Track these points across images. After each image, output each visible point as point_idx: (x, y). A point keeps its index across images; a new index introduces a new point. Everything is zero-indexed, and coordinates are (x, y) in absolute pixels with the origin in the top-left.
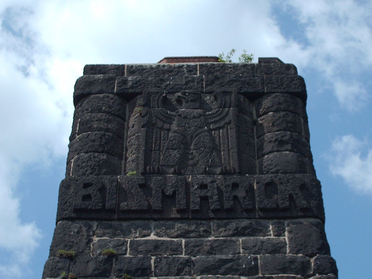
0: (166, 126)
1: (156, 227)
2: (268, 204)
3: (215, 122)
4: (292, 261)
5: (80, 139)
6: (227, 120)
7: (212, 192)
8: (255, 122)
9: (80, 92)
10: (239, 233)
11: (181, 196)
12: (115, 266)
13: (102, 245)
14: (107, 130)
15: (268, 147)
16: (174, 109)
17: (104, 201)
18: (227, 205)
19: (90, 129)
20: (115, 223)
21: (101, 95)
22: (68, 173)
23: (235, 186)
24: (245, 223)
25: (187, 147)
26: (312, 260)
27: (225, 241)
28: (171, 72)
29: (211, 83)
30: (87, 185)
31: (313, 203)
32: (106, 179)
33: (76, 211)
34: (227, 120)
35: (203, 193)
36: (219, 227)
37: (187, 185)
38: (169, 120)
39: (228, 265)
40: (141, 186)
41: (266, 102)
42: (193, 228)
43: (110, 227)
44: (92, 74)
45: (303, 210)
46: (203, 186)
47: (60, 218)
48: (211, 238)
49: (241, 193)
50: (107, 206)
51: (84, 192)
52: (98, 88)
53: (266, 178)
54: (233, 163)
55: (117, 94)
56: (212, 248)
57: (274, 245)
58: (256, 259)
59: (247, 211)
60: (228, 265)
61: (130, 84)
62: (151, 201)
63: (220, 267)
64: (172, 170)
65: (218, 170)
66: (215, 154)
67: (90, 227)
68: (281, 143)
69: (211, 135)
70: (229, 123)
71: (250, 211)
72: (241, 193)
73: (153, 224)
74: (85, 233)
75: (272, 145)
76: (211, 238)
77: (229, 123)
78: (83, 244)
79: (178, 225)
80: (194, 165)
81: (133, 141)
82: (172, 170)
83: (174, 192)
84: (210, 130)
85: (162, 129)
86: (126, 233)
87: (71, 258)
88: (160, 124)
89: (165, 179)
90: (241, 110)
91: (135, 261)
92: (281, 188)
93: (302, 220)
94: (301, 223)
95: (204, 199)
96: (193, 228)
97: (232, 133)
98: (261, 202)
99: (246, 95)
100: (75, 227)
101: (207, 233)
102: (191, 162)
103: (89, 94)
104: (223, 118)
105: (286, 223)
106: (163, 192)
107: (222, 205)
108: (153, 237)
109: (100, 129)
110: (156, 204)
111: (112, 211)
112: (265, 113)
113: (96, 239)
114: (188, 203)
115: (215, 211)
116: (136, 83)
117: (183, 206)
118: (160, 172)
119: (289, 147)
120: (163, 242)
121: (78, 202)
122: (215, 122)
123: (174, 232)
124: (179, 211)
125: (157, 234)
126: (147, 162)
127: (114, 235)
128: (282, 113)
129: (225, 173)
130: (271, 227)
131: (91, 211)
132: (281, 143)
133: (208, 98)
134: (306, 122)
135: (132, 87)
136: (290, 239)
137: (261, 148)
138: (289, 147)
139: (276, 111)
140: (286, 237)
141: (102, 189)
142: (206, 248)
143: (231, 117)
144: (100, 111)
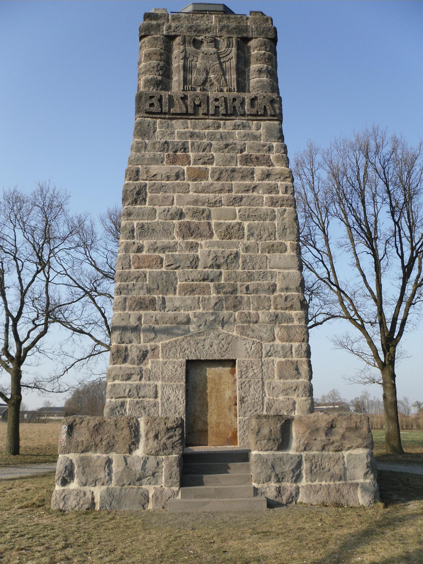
6: (230, 56)
15: (252, 60)
30: (151, 97)
35: (217, 103)
68: (260, 71)
95: (217, 107)
110: (190, 111)
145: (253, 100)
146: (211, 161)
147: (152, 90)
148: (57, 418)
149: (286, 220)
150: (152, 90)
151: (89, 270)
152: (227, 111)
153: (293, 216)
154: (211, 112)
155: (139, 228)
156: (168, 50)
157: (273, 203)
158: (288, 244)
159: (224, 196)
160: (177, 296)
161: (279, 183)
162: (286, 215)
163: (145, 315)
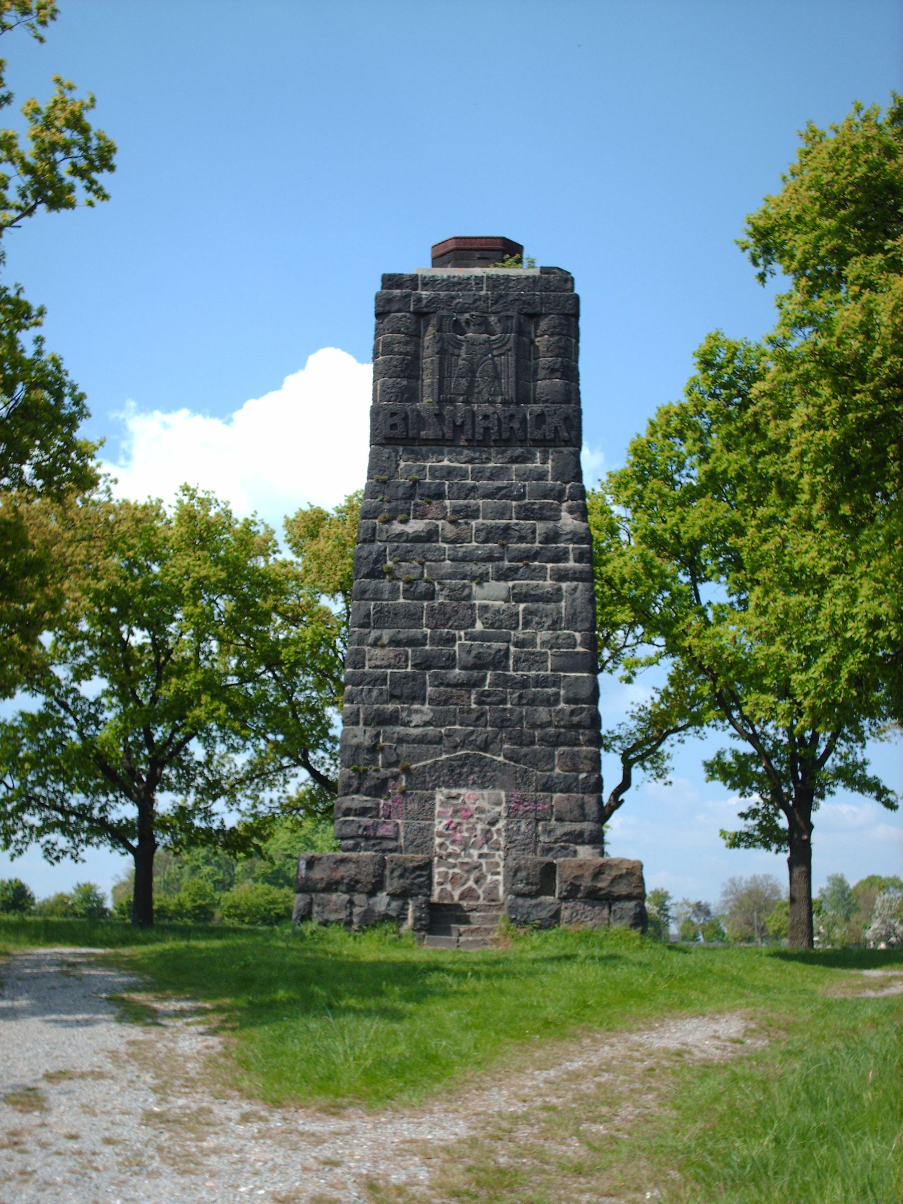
0: (456, 352)
1: (449, 453)
2: (538, 435)
3: (497, 348)
4: (552, 490)
5: (385, 362)
6: (508, 347)
7: (493, 423)
8: (532, 342)
9: (381, 309)
10: (513, 460)
11: (468, 427)
12: (419, 491)
13: (408, 470)
14: (406, 354)
15: (541, 374)
16: (463, 333)
17: (407, 431)
18: (505, 435)
19: (391, 352)
20: (417, 448)
21: (400, 314)
22: (374, 400)
23: (512, 416)
24: (519, 451)
25: (474, 376)
26: (568, 486)
27: (502, 468)
28: (460, 284)
29: (496, 302)
30: (393, 414)
31: (573, 433)
32: (408, 406)
33: (386, 438)
34: (508, 347)
35: (486, 423)
36: (498, 453)
37: (473, 414)
38: (458, 345)
39: (503, 492)
40: (436, 415)
41: (544, 324)
42: (477, 455)
43: (412, 452)
44: (408, 400)
45: (565, 441)
46: (486, 417)
47: (373, 443)
48: (491, 465)
49: (516, 425)
50: (410, 435)
51: (391, 421)
52: (396, 306)
53: (537, 408)
54: (511, 394)
55: (414, 313)
56: (492, 474)
57: (539, 474)
58: (524, 486)
59: (520, 441)
60: (503, 492)
61: (424, 302)
62: (446, 430)
63: (497, 493)
64: (461, 398)
65: (499, 399)
66: (496, 383)
67: (397, 452)
68: (552, 371)
69: (494, 363)
70: (509, 350)
71: (522, 442)
72: (516, 425)
73: (446, 450)
74: (393, 458)
75: (545, 372)
76: (491, 465)
77: (509, 350)
78: (392, 469)
79: (466, 452)
80: (479, 393)
81: (428, 365)
82: (461, 398)
83: (463, 422)
84: (492, 359)
85: (453, 354)
86: (425, 458)
87: (384, 482)
88: (451, 350)
89: (455, 407)
90: (521, 332)
91: (433, 486)
92: (549, 420)
93: (563, 449)
94: (561, 452)
95: (487, 429)
96: (477, 455)
97: (512, 360)
98: (532, 433)
99: (526, 314)
100: (386, 451)
101: (488, 460)
102: (476, 390)
103: (389, 312)
104: (504, 345)
105: (551, 450)
106: (454, 423)
107: (500, 435)
108: (446, 463)
109: (400, 353)
110: (449, 435)
111: (414, 439)
112: (542, 336)
113: (402, 464)
114: (473, 435)
115: (495, 441)
116: (431, 301)
117: (470, 437)
118: (452, 402)
119: (558, 374)
120: (455, 468)
121: (387, 431)
122: (497, 348)
123: (462, 458)
124: (466, 440)
125: (450, 460)
126: (441, 391)
127: (416, 460)
128: (557, 338)
129: (505, 403)
130: (538, 455)
131: (397, 439)
132: (552, 371)
133: (493, 319)
134: (578, 341)
135: (426, 306)
136: (553, 468)
137: (535, 372)
138: (558, 374)
139: (551, 335)
140: (549, 465)
141: (405, 418)
142: (487, 474)
143: (511, 344)
144: (399, 332)
145: (540, 418)
146: (473, 514)
147: (397, 406)
148: (86, 1016)
149: (578, 602)
150: (397, 406)
151: (392, 655)
152: (500, 435)
153: (588, 595)
154: (479, 437)
155: (376, 613)
156: (416, 336)
157: (561, 576)
158: (578, 636)
159: (490, 567)
160: (427, 706)
161: (571, 546)
162: (578, 594)
163: (385, 732)
